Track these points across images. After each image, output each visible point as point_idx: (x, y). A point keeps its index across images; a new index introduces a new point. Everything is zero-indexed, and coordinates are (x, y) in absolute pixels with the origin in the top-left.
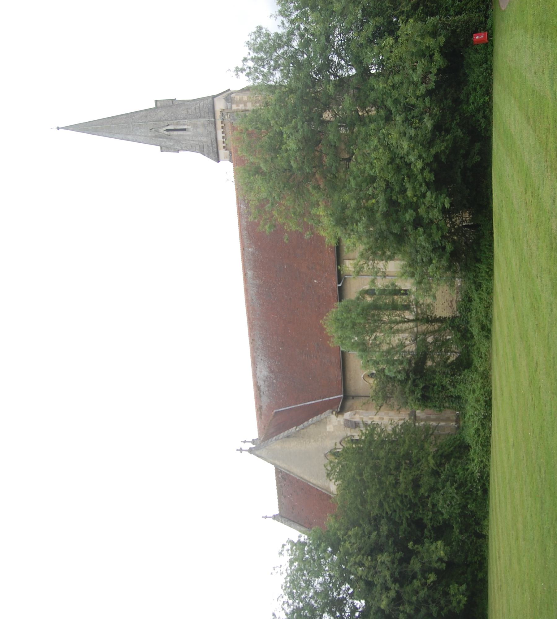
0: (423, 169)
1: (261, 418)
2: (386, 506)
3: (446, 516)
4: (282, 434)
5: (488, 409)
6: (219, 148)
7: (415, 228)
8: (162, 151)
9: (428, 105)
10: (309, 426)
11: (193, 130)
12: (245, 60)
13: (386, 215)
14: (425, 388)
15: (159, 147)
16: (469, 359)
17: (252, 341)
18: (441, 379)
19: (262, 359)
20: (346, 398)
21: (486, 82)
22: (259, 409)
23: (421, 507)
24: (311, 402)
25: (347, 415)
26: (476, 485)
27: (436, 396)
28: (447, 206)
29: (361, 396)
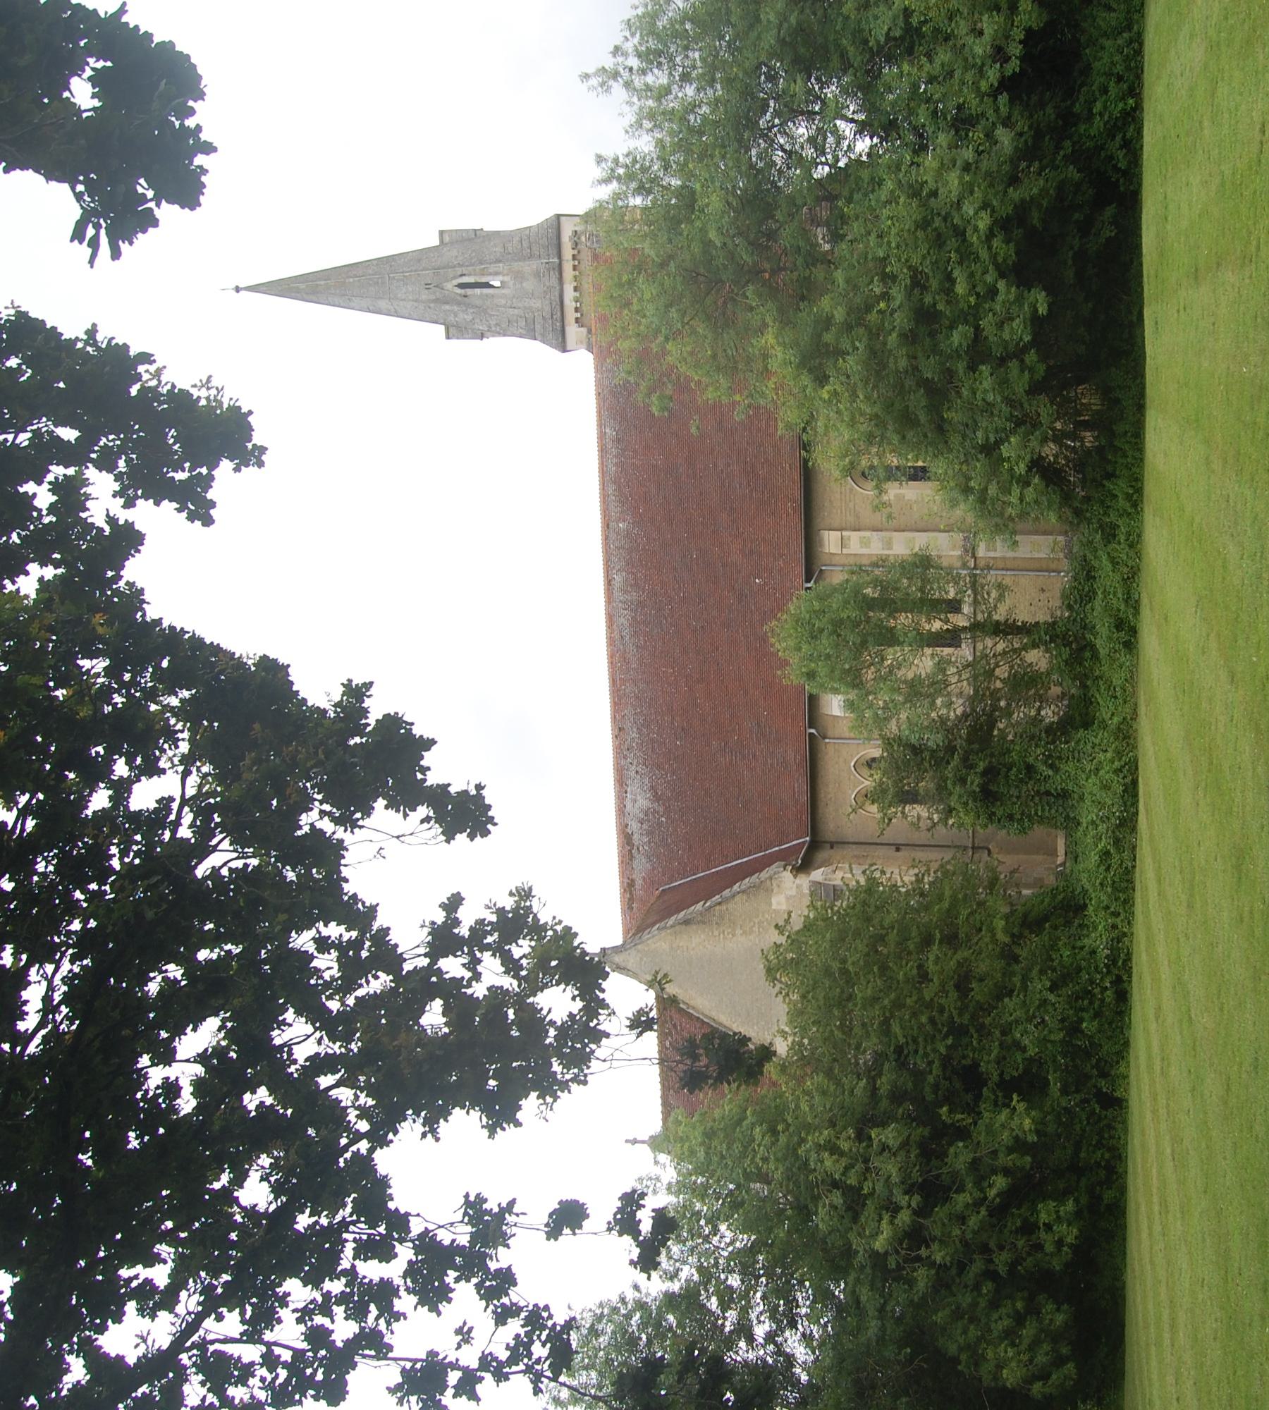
0: (990, 235)
1: (631, 908)
2: (896, 1028)
3: (1032, 1052)
4: (673, 918)
5: (1129, 803)
6: (566, 322)
7: (972, 368)
8: (448, 337)
9: (1004, 110)
10: (733, 896)
11: (515, 284)
12: (617, 51)
13: (909, 338)
14: (989, 773)
15: (442, 328)
16: (1087, 714)
17: (619, 732)
18: (1026, 750)
19: (637, 772)
20: (816, 845)
21: (1128, 69)
22: (628, 887)
23: (975, 1036)
24: (739, 861)
25: (817, 875)
26: (1102, 979)
27: (1014, 791)
28: (1042, 310)
29: (848, 843)
